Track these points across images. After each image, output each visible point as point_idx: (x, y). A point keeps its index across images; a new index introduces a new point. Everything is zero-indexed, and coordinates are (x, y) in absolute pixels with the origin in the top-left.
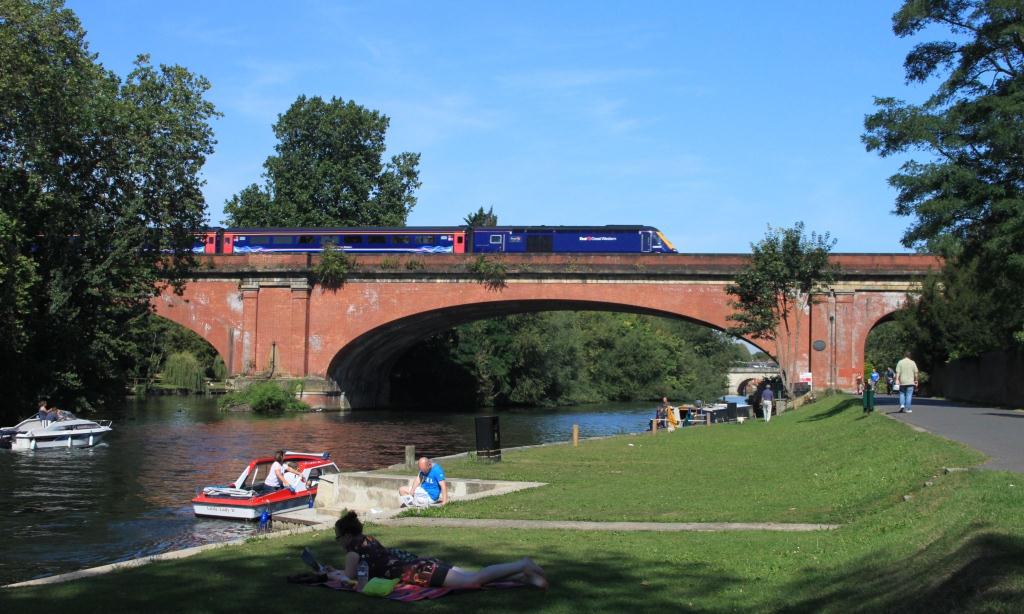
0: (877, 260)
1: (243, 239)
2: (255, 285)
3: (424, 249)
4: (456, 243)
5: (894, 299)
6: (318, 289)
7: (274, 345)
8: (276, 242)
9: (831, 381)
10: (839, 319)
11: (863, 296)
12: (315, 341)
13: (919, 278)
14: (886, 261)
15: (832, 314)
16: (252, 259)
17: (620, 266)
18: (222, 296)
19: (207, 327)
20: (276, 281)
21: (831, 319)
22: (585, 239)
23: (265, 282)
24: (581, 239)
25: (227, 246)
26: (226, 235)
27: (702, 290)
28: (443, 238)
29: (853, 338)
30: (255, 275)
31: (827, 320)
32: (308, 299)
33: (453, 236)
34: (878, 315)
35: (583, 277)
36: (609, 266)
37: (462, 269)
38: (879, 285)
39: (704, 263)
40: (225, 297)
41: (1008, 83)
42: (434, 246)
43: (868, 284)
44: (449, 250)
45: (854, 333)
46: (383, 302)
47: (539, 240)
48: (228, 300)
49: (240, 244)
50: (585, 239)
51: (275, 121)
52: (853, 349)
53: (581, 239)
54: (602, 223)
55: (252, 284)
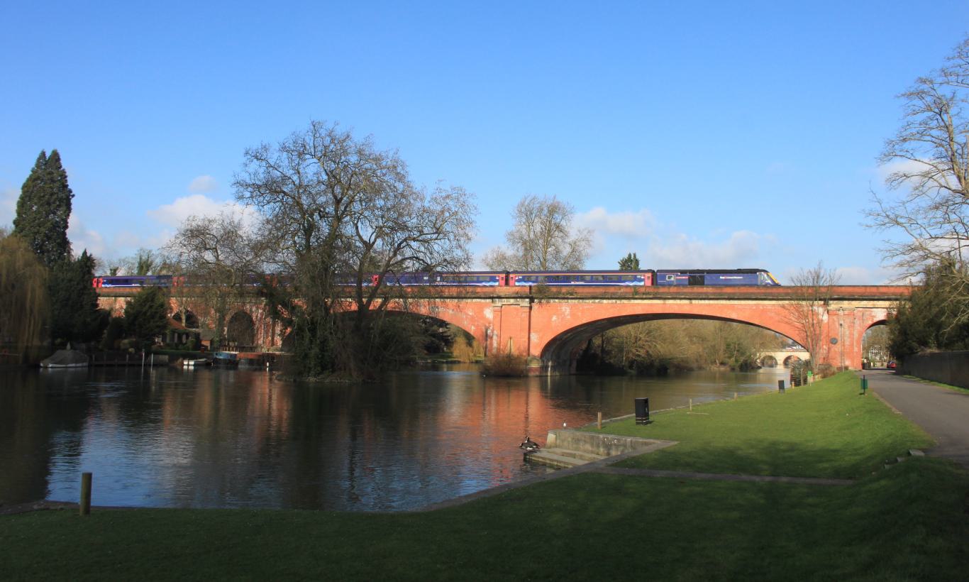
0: (868, 290)
1: (521, 277)
2: (500, 304)
3: (627, 283)
4: (500, 281)
5: (880, 312)
6: (535, 306)
7: (511, 338)
8: (481, 279)
9: (841, 363)
10: (846, 326)
11: (859, 311)
12: (534, 337)
13: (896, 300)
14: (874, 290)
15: (842, 322)
16: (498, 289)
17: (714, 294)
18: (482, 308)
19: (473, 328)
20: (512, 301)
21: (841, 325)
22: (723, 278)
23: (505, 301)
24: (721, 278)
25: (511, 282)
26: (511, 275)
27: (761, 308)
28: (638, 277)
29: (855, 337)
30: (500, 298)
31: (837, 326)
32: (530, 312)
33: (644, 276)
34: (870, 323)
35: (690, 299)
36: (706, 293)
37: (589, 295)
38: (870, 304)
39: (763, 291)
40: (482, 311)
41: (923, 345)
42: (633, 281)
43: (864, 303)
44: (642, 284)
45: (855, 333)
46: (572, 314)
47: (696, 278)
48: (485, 312)
49: (519, 281)
50: (723, 278)
51: (58, 152)
52: (855, 344)
53: (721, 278)
54: (735, 268)
55: (498, 303)
